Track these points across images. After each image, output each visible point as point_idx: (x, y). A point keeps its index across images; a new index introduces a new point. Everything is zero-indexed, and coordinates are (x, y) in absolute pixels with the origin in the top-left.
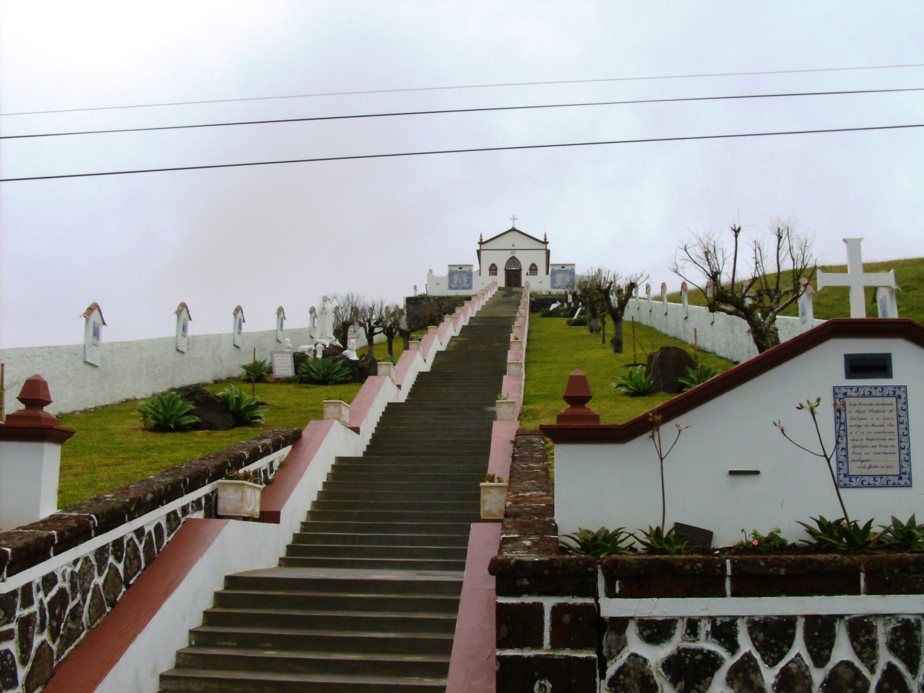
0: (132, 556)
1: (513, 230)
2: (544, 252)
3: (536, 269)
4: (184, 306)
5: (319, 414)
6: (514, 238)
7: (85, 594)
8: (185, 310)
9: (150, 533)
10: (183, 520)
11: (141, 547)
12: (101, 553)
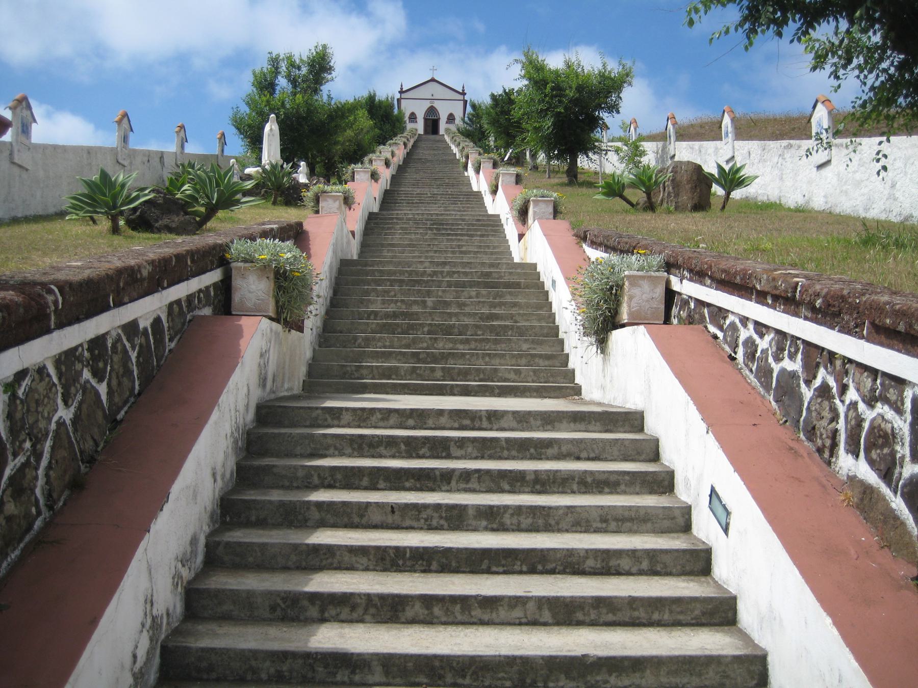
0: (121, 371)
1: (433, 80)
4: (125, 115)
7: (37, 441)
8: (125, 120)
9: (146, 329)
10: (189, 317)
11: (133, 355)
12: (67, 359)
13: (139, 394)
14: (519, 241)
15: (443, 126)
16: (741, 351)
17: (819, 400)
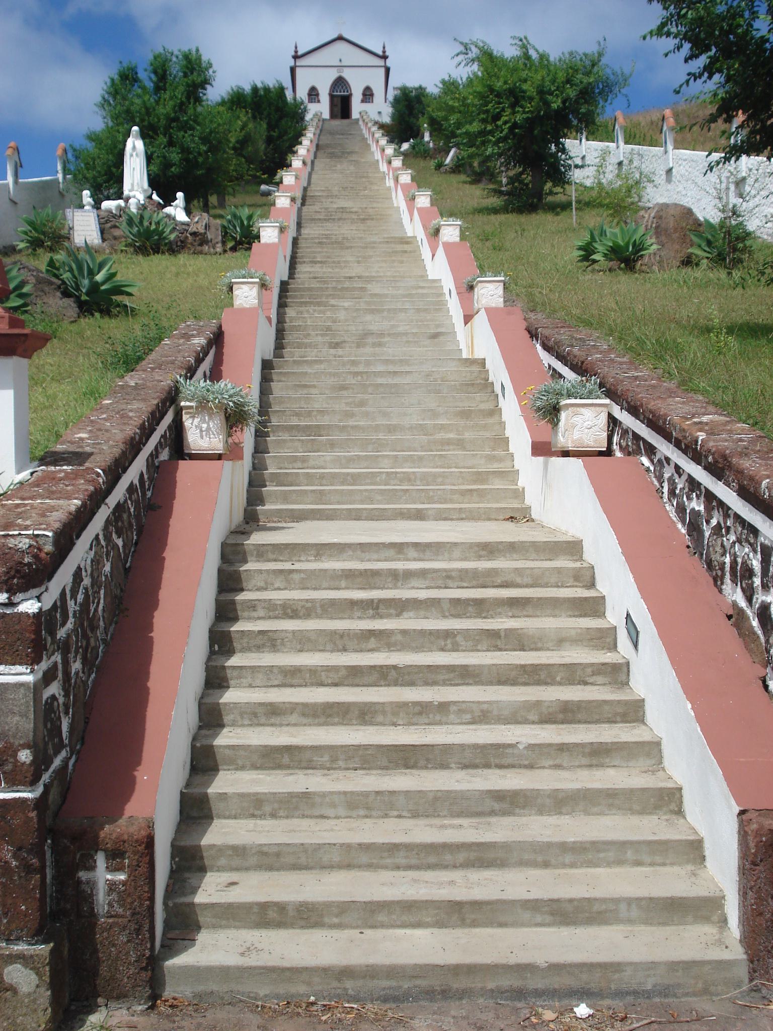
1: (340, 38)
2: (383, 70)
3: (372, 95)
5: (211, 416)
6: (341, 46)
13: (136, 543)
14: (466, 323)
15: (357, 107)
16: (666, 485)
17: (715, 537)
